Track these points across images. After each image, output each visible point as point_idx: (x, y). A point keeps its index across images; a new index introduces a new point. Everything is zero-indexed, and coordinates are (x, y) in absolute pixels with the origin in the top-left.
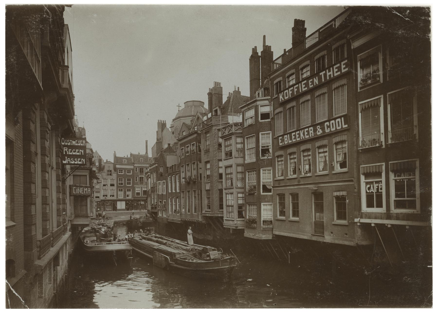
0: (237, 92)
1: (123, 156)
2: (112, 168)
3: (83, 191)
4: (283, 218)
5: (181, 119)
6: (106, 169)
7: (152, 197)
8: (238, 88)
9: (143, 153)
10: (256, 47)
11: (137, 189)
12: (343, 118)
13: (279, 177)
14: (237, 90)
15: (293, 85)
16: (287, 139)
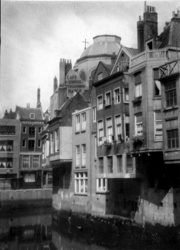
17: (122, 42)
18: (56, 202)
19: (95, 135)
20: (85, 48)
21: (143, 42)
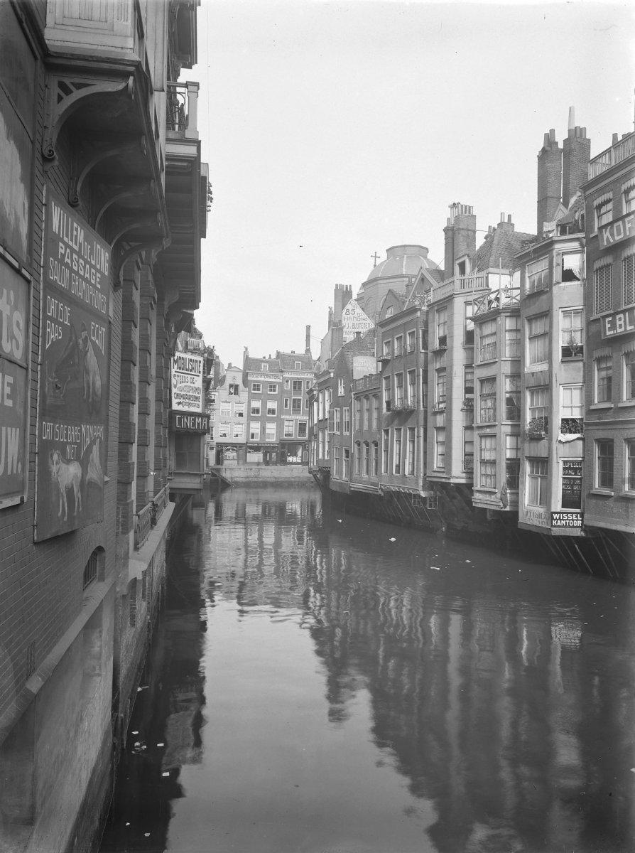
0: (506, 225)
1: (260, 357)
2: (239, 381)
3: (194, 424)
4: (605, 491)
5: (379, 282)
6: (229, 381)
7: (320, 440)
8: (509, 216)
9: (300, 350)
10: (552, 131)
11: (286, 423)
12: (627, 314)
13: (597, 403)
14: (506, 221)
15: (611, 224)
16: (622, 322)
17: (429, 256)
18: (89, 725)
19: (539, 327)
20: (375, 266)
21: (40, 30)
